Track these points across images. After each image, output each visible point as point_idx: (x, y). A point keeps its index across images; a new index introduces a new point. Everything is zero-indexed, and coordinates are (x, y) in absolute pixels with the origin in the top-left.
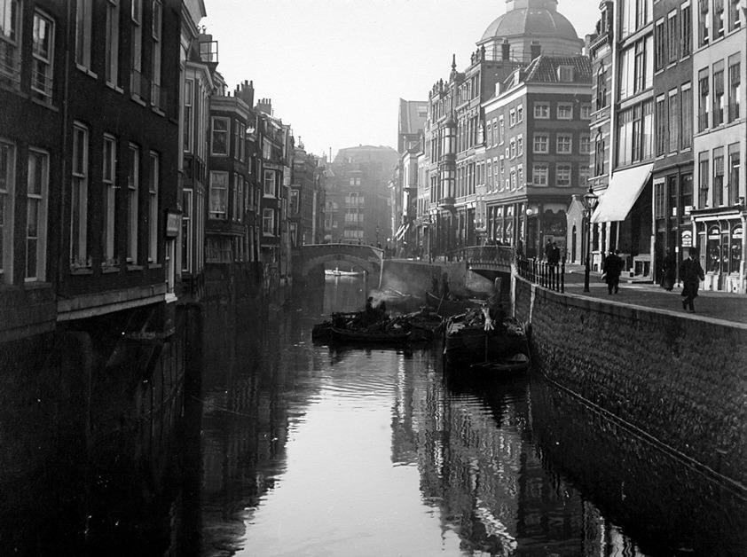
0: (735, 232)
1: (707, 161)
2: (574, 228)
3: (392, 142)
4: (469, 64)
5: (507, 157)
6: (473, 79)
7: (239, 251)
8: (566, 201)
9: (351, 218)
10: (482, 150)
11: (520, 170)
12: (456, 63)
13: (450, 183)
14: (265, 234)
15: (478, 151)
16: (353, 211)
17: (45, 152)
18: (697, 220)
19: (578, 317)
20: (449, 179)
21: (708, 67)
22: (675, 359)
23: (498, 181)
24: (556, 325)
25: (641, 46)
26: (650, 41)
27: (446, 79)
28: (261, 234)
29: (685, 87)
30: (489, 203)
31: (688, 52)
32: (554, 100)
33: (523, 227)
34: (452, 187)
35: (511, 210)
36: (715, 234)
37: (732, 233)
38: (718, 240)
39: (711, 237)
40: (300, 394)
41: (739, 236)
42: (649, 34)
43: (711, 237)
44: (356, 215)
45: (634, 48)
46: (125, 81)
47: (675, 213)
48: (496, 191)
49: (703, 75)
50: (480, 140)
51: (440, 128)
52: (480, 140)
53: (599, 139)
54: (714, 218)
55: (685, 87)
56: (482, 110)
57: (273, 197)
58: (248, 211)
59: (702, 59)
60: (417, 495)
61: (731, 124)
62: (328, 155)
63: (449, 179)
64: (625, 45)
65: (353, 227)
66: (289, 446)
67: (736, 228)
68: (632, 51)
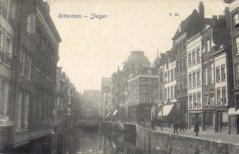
1: (192, 96)
3: (100, 89)
4: (123, 69)
6: (124, 72)
8: (151, 106)
10: (127, 92)
22: (191, 149)
23: (132, 99)
27: (116, 72)
29: (185, 77)
31: (185, 66)
32: (146, 79)
35: (135, 109)
44: (89, 109)
48: (168, 60)
50: (126, 89)
51: (115, 86)
52: (126, 89)
53: (161, 90)
55: (185, 77)
56: (127, 81)
57: (70, 104)
58: (35, 12)
59: (190, 70)
65: (88, 112)
66: (192, 13)
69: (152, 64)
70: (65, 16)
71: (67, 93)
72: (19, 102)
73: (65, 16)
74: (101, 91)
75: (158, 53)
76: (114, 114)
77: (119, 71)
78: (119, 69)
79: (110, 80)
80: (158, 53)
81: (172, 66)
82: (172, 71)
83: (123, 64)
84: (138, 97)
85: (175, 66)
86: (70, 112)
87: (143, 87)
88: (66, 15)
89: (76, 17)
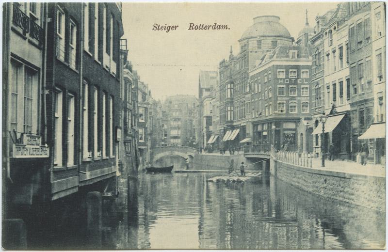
2: (302, 134)
5: (263, 98)
9: (174, 133)
14: (140, 141)
15: (247, 96)
16: (175, 129)
17: (73, 95)
19: (322, 180)
20: (231, 111)
21: (381, 48)
24: (309, 184)
27: (227, 59)
28: (138, 141)
30: (253, 123)
34: (232, 114)
40: (5, 220)
46: (74, 64)
55: (367, 59)
57: (143, 121)
61: (381, 82)
63: (231, 111)
69: (296, 41)
70: (201, 27)
71: (137, 102)
72: (259, 237)
73: (201, 27)
74: (198, 97)
75: (307, 19)
76: (224, 138)
77: (231, 58)
78: (231, 52)
79: (214, 75)
80: (307, 19)
81: (341, 38)
82: (341, 48)
83: (239, 43)
84: (271, 105)
85: (347, 38)
86: (143, 137)
87: (281, 84)
88: (203, 26)
89: (219, 27)
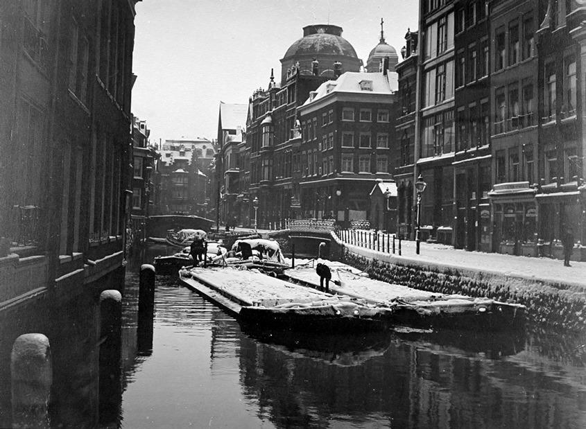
0: (529, 212)
7: (72, 200)
11: (331, 160)
12: (274, 76)
13: (269, 169)
18: (495, 202)
20: (269, 166)
25: (441, 69)
26: (451, 66)
27: (266, 88)
33: (342, 417)
36: (510, 213)
37: (526, 213)
38: (513, 218)
39: (506, 216)
41: (533, 215)
42: (449, 12)
43: (506, 216)
45: (436, 24)
47: (476, 225)
49: (499, 32)
53: (404, 138)
54: (512, 201)
60: (239, 389)
62: (159, 144)
64: (426, 68)
67: (529, 208)
68: (435, 26)
